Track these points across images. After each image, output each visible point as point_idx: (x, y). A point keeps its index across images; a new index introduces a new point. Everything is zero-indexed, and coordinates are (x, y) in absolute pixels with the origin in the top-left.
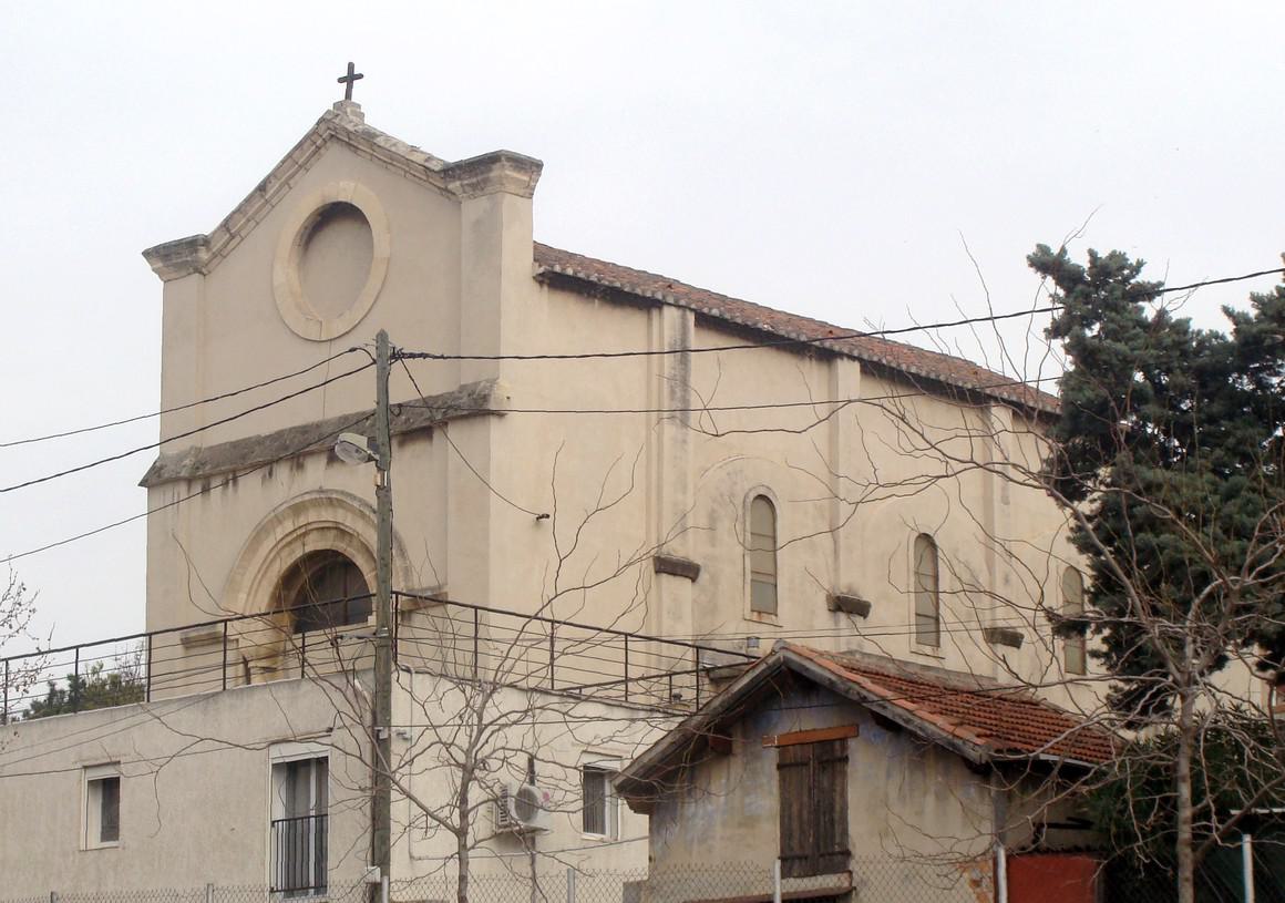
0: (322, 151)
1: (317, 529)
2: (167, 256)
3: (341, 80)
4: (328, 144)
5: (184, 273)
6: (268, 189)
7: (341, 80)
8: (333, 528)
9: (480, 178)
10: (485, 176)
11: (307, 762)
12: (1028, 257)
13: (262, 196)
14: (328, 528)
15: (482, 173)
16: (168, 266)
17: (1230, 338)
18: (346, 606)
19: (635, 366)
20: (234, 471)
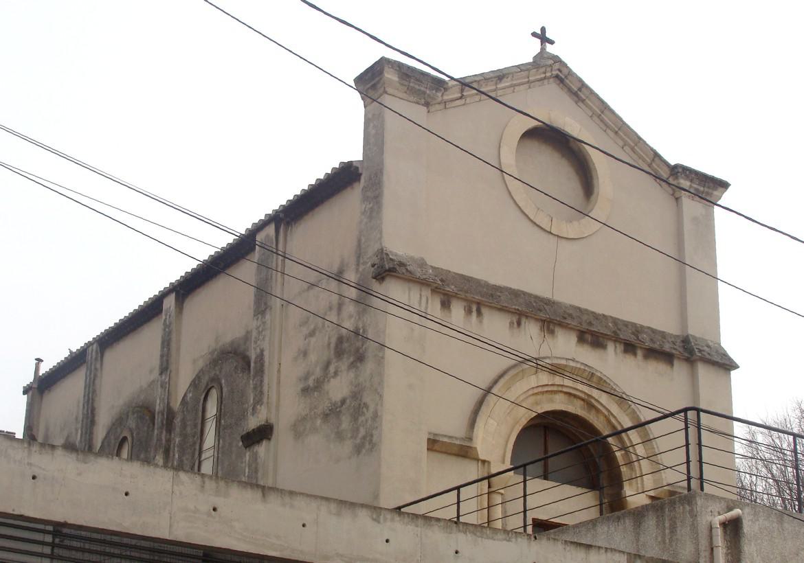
0: (546, 81)
1: (566, 393)
2: (407, 75)
3: (543, 30)
4: (551, 80)
5: (412, 98)
6: (503, 81)
7: (543, 30)
8: (583, 400)
9: (706, 190)
10: (710, 191)
11: (115, 447)
12: (736, 367)
13: (584, 100)
14: (575, 396)
15: (709, 188)
16: (402, 85)
17: (174, 294)
18: (546, 451)
19: (412, 294)
20: (479, 304)
